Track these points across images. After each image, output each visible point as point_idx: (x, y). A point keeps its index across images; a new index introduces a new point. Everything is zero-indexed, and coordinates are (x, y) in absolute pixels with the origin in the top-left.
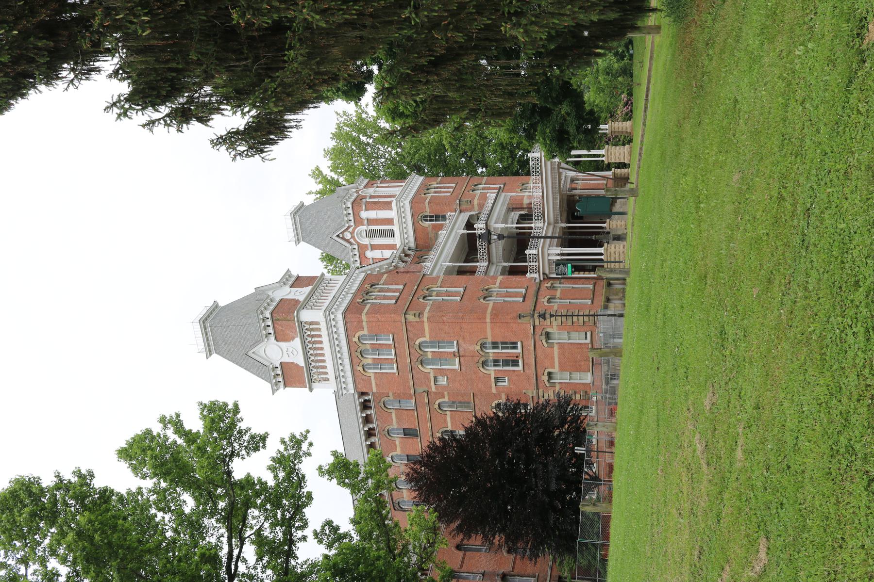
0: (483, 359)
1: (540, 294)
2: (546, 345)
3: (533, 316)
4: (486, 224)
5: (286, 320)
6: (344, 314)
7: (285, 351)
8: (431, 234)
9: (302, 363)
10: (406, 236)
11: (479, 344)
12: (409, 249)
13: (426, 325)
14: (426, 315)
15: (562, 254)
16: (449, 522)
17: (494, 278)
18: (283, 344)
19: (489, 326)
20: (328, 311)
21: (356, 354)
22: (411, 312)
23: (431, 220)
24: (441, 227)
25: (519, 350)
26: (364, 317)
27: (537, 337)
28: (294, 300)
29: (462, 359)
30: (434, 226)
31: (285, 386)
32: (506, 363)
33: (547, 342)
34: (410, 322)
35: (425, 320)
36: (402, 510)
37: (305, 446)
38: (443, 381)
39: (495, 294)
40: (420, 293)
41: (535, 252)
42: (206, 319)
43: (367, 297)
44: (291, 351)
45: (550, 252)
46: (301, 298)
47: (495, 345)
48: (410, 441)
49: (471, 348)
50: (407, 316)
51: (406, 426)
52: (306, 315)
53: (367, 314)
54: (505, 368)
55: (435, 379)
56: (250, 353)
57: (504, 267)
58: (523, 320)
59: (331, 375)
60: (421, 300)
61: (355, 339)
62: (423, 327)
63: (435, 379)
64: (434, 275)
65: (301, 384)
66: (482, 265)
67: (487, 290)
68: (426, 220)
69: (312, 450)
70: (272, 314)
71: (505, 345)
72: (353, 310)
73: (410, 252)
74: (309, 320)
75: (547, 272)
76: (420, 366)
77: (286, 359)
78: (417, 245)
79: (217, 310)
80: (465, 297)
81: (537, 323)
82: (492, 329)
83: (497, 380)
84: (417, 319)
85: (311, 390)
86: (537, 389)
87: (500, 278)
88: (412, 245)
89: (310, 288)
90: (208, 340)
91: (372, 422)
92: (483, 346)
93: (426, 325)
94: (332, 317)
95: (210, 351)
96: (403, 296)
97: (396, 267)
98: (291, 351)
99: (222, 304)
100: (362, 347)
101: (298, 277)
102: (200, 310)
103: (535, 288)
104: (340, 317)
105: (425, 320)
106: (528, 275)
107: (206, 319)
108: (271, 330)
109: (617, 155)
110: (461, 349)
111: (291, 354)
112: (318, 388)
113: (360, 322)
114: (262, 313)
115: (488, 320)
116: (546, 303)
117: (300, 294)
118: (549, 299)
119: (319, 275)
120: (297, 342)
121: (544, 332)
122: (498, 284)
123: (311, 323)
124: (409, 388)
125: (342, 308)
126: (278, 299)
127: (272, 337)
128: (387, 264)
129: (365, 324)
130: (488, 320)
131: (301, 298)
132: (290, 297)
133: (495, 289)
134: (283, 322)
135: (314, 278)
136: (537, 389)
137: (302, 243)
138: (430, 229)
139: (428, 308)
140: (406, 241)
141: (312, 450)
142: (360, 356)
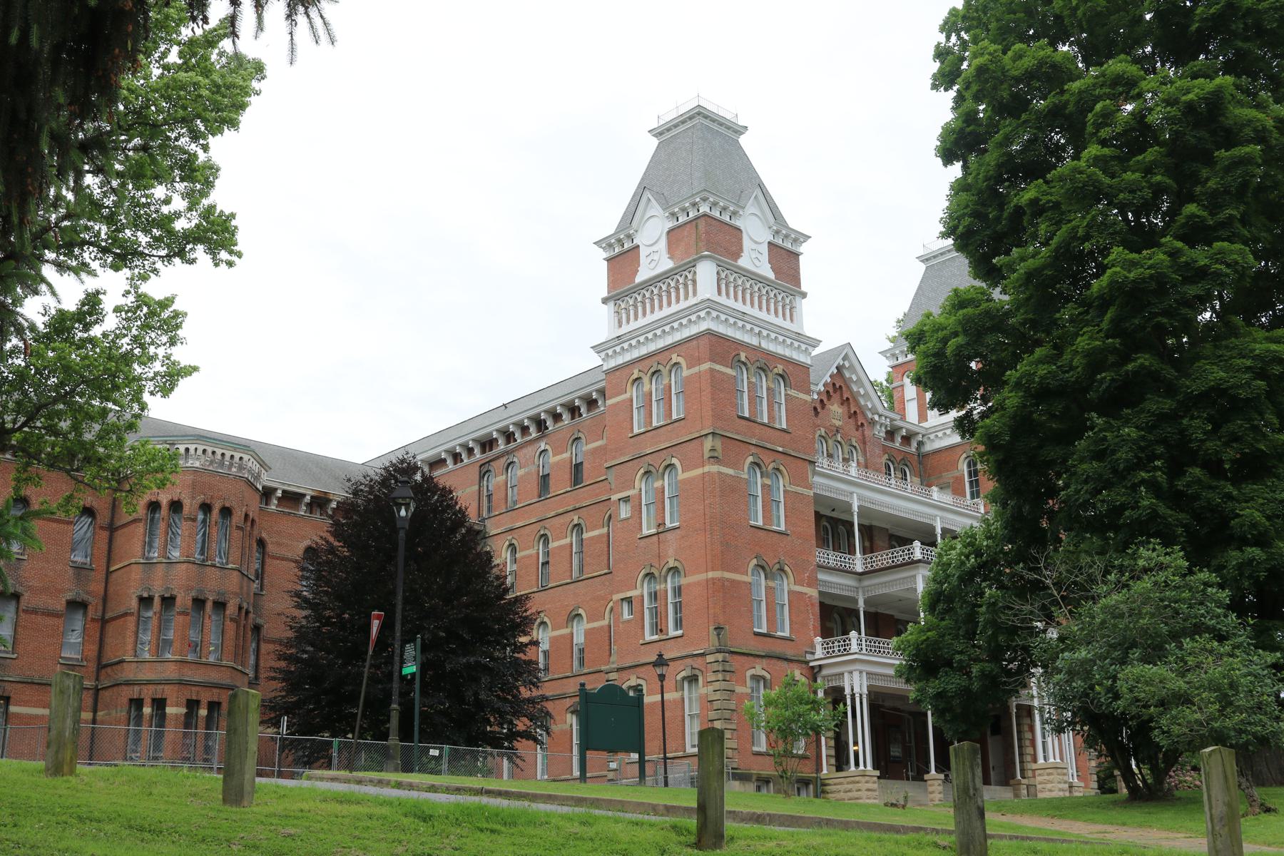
0: (657, 574)
1: (774, 661)
2: (679, 677)
3: (719, 651)
4: (919, 561)
5: (698, 239)
6: (709, 333)
7: (655, 248)
8: (948, 476)
9: (638, 279)
10: (940, 434)
11: (677, 564)
12: (920, 444)
13: (699, 471)
14: (715, 468)
15: (853, 696)
16: (337, 531)
17: (813, 582)
18: (663, 244)
19: (702, 577)
20: (709, 305)
21: (655, 365)
22: (718, 444)
23: (970, 473)
24: (958, 492)
25: (672, 632)
26: (706, 366)
27: (689, 661)
28: (741, 250)
29: (655, 538)
30: (960, 480)
31: (608, 260)
32: (655, 613)
33: (684, 679)
34: (702, 445)
35: (706, 469)
36: (481, 477)
37: (224, 255)
38: (625, 512)
39: (771, 584)
40: (766, 458)
41: (854, 648)
42: (706, 117)
43: (752, 369)
44: (655, 259)
45: (856, 675)
46: (744, 262)
47: (678, 591)
48: (566, 475)
49: (671, 552)
50: (710, 437)
51: (585, 465)
52: (706, 272)
53: (712, 370)
54: (647, 612)
55: (626, 500)
56: (647, 194)
57: (856, 601)
58: (713, 633)
59: (626, 329)
60: (750, 459)
61: (675, 358)
62: (696, 467)
63: (626, 500)
64: (817, 479)
65: (612, 283)
66: (858, 562)
67: (782, 570)
68: (969, 466)
69: (223, 266)
70: (705, 215)
71: (678, 607)
72: (720, 348)
73: (914, 444)
74: (698, 278)
75: (825, 672)
76: (642, 471)
77: (643, 252)
78: (927, 455)
79: (729, 133)
80: (761, 533)
81: (710, 658)
82: (698, 583)
83: (629, 600)
84: (707, 455)
85: (605, 301)
86: (618, 670)
87: (813, 593)
88: (929, 447)
89: (771, 275)
90: (676, 126)
91: (589, 410)
92: (675, 570)
93: (699, 471)
94: (702, 314)
95: (661, 134)
96: (758, 429)
97: (872, 423)
98: (655, 259)
99: (743, 140)
100: (665, 371)
101: (796, 255)
102: (723, 105)
103: (790, 652)
104: (703, 326)
105: (706, 469)
106: (819, 639)
107: (706, 117)
108: (682, 219)
109: (1049, 786)
110: (668, 535)
111: (649, 259)
112: (606, 311)
113: (699, 361)
114: (704, 200)
115: (711, 575)
116: (752, 672)
117: (754, 258)
118: (764, 678)
119: (804, 288)
120: (667, 264)
121: (697, 672)
122: (798, 588)
123: (694, 281)
124: (614, 458)
125: (721, 329)
126: (738, 223)
127: (671, 224)
128: (874, 406)
129: (696, 370)
130: (711, 575)
131: (744, 262)
132: (746, 243)
133: (787, 586)
134: (694, 236)
135: (796, 279)
136: (618, 670)
137: (922, 267)
138: (956, 474)
139: (731, 472)
140: (932, 436)
141: (223, 266)
142: (652, 370)
